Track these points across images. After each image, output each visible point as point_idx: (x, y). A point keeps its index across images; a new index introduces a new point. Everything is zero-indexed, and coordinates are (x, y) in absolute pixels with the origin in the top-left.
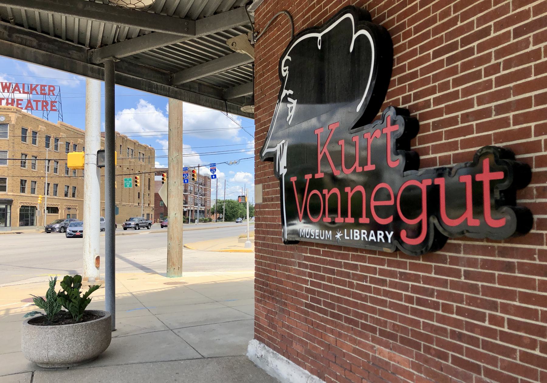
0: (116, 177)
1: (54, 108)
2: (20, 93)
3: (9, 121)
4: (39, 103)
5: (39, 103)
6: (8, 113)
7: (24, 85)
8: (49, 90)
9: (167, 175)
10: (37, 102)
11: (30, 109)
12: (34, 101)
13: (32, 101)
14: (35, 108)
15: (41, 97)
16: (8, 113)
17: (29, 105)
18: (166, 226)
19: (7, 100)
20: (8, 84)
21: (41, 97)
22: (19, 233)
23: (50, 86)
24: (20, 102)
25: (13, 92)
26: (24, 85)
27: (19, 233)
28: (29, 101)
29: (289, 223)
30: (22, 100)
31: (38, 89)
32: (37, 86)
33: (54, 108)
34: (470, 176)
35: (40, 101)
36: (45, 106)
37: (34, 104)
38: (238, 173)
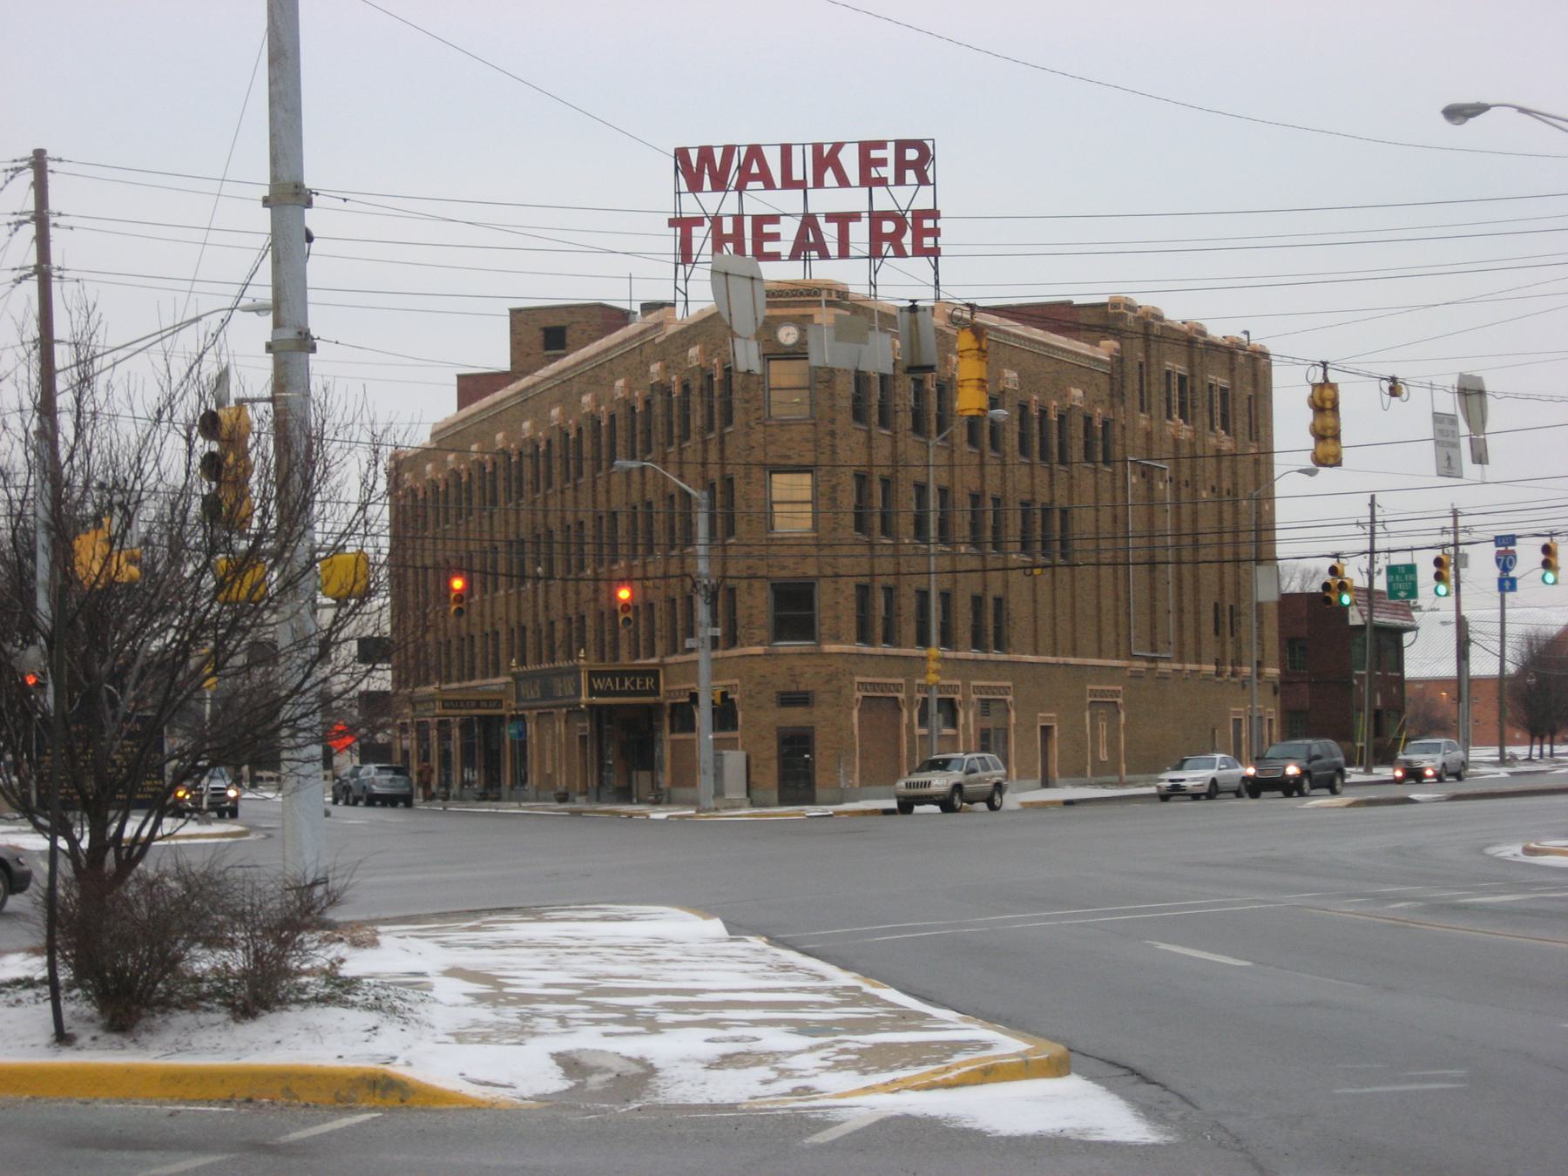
1: (768, 247)
2: (769, 185)
4: (696, 231)
5: (696, 231)
6: (809, 311)
7: (786, 150)
8: (901, 165)
9: (1207, 678)
10: (843, 220)
11: (814, 254)
12: (830, 217)
13: (821, 220)
14: (833, 249)
15: (854, 199)
16: (809, 311)
19: (717, 221)
20: (718, 155)
21: (854, 199)
22: (487, 1084)
23: (902, 146)
24: (767, 228)
25: (741, 188)
26: (786, 150)
27: (487, 1084)
28: (809, 221)
30: (774, 219)
31: (850, 160)
32: (837, 147)
33: (768, 247)
34: (775, 477)
35: (856, 216)
36: (888, 237)
37: (830, 231)
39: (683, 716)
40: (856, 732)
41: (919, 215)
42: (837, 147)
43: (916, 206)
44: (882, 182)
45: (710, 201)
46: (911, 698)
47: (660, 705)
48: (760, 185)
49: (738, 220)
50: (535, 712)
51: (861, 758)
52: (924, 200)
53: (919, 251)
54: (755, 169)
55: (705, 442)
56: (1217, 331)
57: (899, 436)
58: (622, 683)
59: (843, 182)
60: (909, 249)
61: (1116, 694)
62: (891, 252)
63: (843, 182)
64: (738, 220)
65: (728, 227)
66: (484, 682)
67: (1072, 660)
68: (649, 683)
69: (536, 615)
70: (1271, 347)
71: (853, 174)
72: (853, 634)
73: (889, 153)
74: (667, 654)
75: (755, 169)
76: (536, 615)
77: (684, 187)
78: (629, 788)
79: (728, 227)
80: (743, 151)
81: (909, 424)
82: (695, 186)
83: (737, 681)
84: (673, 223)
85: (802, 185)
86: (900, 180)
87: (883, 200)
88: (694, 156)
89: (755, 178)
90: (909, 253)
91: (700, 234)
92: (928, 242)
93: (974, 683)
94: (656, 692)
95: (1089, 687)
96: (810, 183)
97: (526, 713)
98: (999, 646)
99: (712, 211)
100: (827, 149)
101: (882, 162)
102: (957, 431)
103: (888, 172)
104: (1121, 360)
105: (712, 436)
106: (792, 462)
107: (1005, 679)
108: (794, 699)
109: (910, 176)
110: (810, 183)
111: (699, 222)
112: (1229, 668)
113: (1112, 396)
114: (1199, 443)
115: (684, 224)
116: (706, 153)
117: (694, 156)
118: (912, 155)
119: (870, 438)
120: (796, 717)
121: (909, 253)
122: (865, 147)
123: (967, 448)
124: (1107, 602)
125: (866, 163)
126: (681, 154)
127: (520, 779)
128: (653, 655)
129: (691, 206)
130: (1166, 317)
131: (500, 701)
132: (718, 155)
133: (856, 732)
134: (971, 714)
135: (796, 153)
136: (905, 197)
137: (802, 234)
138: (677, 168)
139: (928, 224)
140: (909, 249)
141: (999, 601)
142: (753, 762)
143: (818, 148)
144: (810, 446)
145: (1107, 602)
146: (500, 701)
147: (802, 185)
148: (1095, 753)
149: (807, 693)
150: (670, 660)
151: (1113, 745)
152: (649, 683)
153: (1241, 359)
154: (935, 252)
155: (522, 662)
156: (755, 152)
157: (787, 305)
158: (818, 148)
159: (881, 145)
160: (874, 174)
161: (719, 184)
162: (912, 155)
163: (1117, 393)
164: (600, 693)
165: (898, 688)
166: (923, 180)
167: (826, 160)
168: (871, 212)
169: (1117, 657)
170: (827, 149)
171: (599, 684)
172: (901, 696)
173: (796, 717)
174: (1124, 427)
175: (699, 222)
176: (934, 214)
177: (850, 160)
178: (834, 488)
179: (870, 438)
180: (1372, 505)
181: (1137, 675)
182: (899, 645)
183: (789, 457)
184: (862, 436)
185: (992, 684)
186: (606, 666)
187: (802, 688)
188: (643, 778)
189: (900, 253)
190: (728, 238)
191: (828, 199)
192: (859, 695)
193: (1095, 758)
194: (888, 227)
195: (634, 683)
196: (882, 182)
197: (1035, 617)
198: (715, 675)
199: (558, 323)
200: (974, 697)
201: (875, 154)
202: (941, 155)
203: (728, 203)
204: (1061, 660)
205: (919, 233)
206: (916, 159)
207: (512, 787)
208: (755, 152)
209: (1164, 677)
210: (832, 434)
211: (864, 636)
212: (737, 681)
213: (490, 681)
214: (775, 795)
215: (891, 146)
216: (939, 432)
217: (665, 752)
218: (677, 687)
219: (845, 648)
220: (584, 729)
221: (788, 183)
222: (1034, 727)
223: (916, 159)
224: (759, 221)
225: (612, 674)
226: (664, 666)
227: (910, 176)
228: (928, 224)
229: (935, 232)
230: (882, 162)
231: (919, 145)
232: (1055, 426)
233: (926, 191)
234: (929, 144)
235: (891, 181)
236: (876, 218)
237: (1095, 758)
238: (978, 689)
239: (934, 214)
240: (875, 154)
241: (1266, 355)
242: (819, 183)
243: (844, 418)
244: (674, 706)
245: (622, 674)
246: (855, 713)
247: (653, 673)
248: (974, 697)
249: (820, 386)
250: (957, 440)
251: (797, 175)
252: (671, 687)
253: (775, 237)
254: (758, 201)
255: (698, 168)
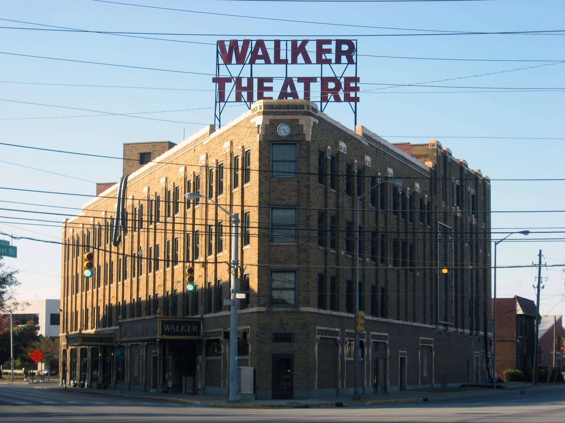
0: (116, 211)
2: (268, 62)
3: (298, 135)
4: (227, 84)
5: (227, 84)
6: (296, 117)
7: (277, 43)
8: (339, 53)
10: (307, 81)
12: (300, 80)
13: (295, 83)
15: (313, 70)
16: (296, 117)
17: (289, 90)
18: (376, 392)
19: (239, 80)
20: (240, 44)
21: (313, 70)
23: (339, 43)
24: (266, 85)
25: (252, 62)
26: (277, 43)
28: (288, 82)
29: (30, 323)
30: (270, 80)
31: (311, 48)
32: (305, 42)
35: (314, 80)
38: (508, 282)
39: (213, 346)
40: (316, 358)
41: (348, 80)
42: (305, 42)
43: (347, 75)
44: (329, 62)
45: (235, 70)
46: (343, 339)
47: (200, 341)
48: (263, 61)
49: (250, 80)
50: (130, 344)
51: (318, 373)
52: (350, 72)
53: (348, 99)
54: (260, 53)
55: (231, 194)
56: (473, 167)
57: (340, 194)
58: (180, 328)
59: (308, 61)
60: (342, 98)
61: (431, 342)
62: (332, 99)
63: (308, 61)
64: (250, 80)
65: (244, 83)
66: (104, 329)
67: (414, 324)
68: (195, 328)
69: (131, 294)
70: (491, 178)
71: (313, 57)
72: (316, 302)
73: (333, 46)
74: (205, 313)
75: (260, 53)
76: (131, 294)
77: (221, 61)
78: (181, 385)
79: (244, 83)
80: (254, 43)
81: (345, 189)
82: (228, 61)
83: (249, 327)
84: (214, 80)
85: (285, 62)
86: (338, 61)
87: (327, 71)
88: (227, 44)
89: (260, 57)
90: (342, 99)
91: (229, 86)
92: (352, 94)
93: (372, 333)
94: (198, 333)
95: (421, 338)
96: (290, 62)
97: (125, 344)
98: (383, 316)
99: (235, 74)
100: (299, 43)
101: (329, 51)
102: (366, 196)
103: (332, 56)
104: (435, 172)
105: (236, 189)
106: (284, 203)
107: (385, 332)
108: (286, 338)
109: (344, 59)
110: (290, 62)
111: (229, 80)
112: (475, 332)
113: (431, 190)
114: (464, 219)
115: (220, 82)
116: (234, 43)
117: (227, 44)
118: (345, 48)
119: (326, 193)
120: (283, 348)
121: (342, 99)
122: (320, 43)
123: (370, 205)
124: (428, 294)
125: (320, 51)
126: (221, 44)
127: (121, 377)
128: (197, 313)
129: (224, 73)
130: (453, 156)
131: (112, 339)
132: (240, 44)
133: (316, 358)
134: (370, 349)
135: (283, 45)
136: (341, 70)
137: (284, 88)
138: (218, 51)
139: (352, 85)
140: (342, 98)
141: (383, 290)
142: (257, 373)
143: (294, 43)
144: (295, 193)
145: (428, 294)
146: (112, 339)
147: (285, 62)
148: (422, 372)
149: (290, 334)
150: (207, 316)
151: (429, 370)
152: (195, 328)
153: (480, 182)
154: (356, 100)
155: (124, 317)
156: (260, 44)
157: (284, 114)
158: (294, 43)
159: (329, 42)
160: (324, 58)
161: (240, 60)
162: (345, 48)
163: (433, 190)
164: (167, 333)
165: (337, 333)
166: (350, 61)
167: (298, 49)
168: (322, 78)
169: (431, 324)
170: (299, 43)
171: (167, 328)
172: (339, 338)
173: (283, 348)
174: (436, 206)
175: (229, 80)
176: (356, 79)
177: (311, 48)
178: (308, 218)
179: (326, 193)
180: (540, 255)
181: (440, 333)
182: (338, 310)
183: (283, 200)
184: (321, 190)
185: (380, 334)
186: (170, 318)
187: (287, 331)
188: (187, 381)
189: (337, 99)
190: (244, 89)
191: (299, 70)
192: (318, 337)
193: (422, 375)
194: (331, 85)
195: (186, 328)
196: (329, 62)
197: (398, 300)
198: (239, 323)
199: (148, 151)
200: (372, 341)
201: (325, 47)
202: (361, 49)
203: (244, 71)
204: (409, 323)
205: (348, 89)
206: (347, 50)
207: (116, 383)
208: (260, 44)
209: (450, 334)
210: (308, 187)
211: (321, 304)
212: (249, 327)
213: (107, 328)
214: (270, 393)
215: (334, 43)
216: (359, 194)
217: (200, 368)
218: (210, 331)
219: (312, 310)
220: (156, 353)
221: (278, 61)
222: (398, 358)
223: (347, 50)
224: (261, 81)
225: (175, 323)
226: (202, 319)
227: (344, 59)
228: (352, 85)
229: (356, 89)
230: (329, 51)
231: (349, 43)
232: (408, 201)
233: (352, 67)
234: (354, 42)
235: (333, 61)
236: (325, 81)
237: (422, 375)
238: (374, 337)
239: (356, 79)
240: (325, 47)
241: (489, 181)
242: (294, 61)
243: (314, 179)
244: (208, 341)
245: (180, 323)
246: (316, 347)
247: (197, 323)
248: (372, 341)
249: (301, 160)
250: (366, 200)
251: (283, 57)
252: (207, 331)
253: (270, 89)
254: (261, 70)
255: (230, 51)
